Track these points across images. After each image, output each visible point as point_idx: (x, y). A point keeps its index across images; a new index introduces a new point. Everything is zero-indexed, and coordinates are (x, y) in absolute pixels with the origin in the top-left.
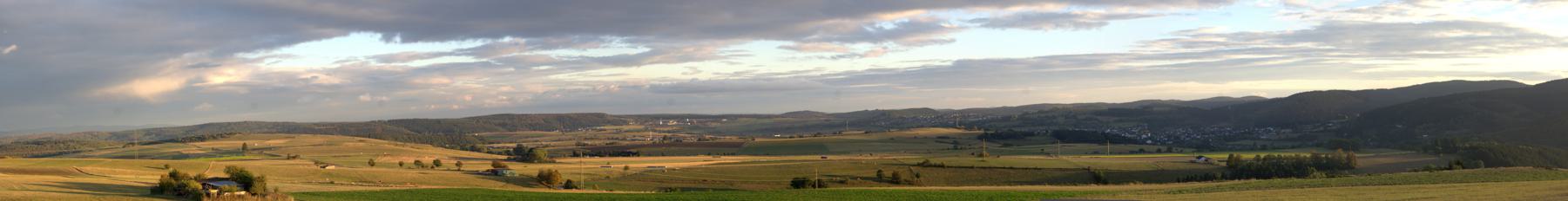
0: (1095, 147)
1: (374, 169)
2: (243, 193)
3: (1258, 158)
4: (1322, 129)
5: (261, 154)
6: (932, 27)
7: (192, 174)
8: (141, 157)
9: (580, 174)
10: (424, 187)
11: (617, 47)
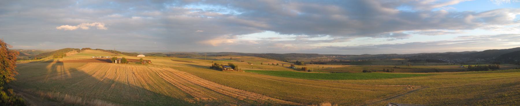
0: (436, 63)
1: (262, 65)
2: (232, 69)
3: (475, 66)
4: (491, 59)
5: (235, 60)
6: (405, 35)
7: (220, 64)
8: (206, 59)
9: (312, 68)
10: (274, 70)
11: (327, 37)
